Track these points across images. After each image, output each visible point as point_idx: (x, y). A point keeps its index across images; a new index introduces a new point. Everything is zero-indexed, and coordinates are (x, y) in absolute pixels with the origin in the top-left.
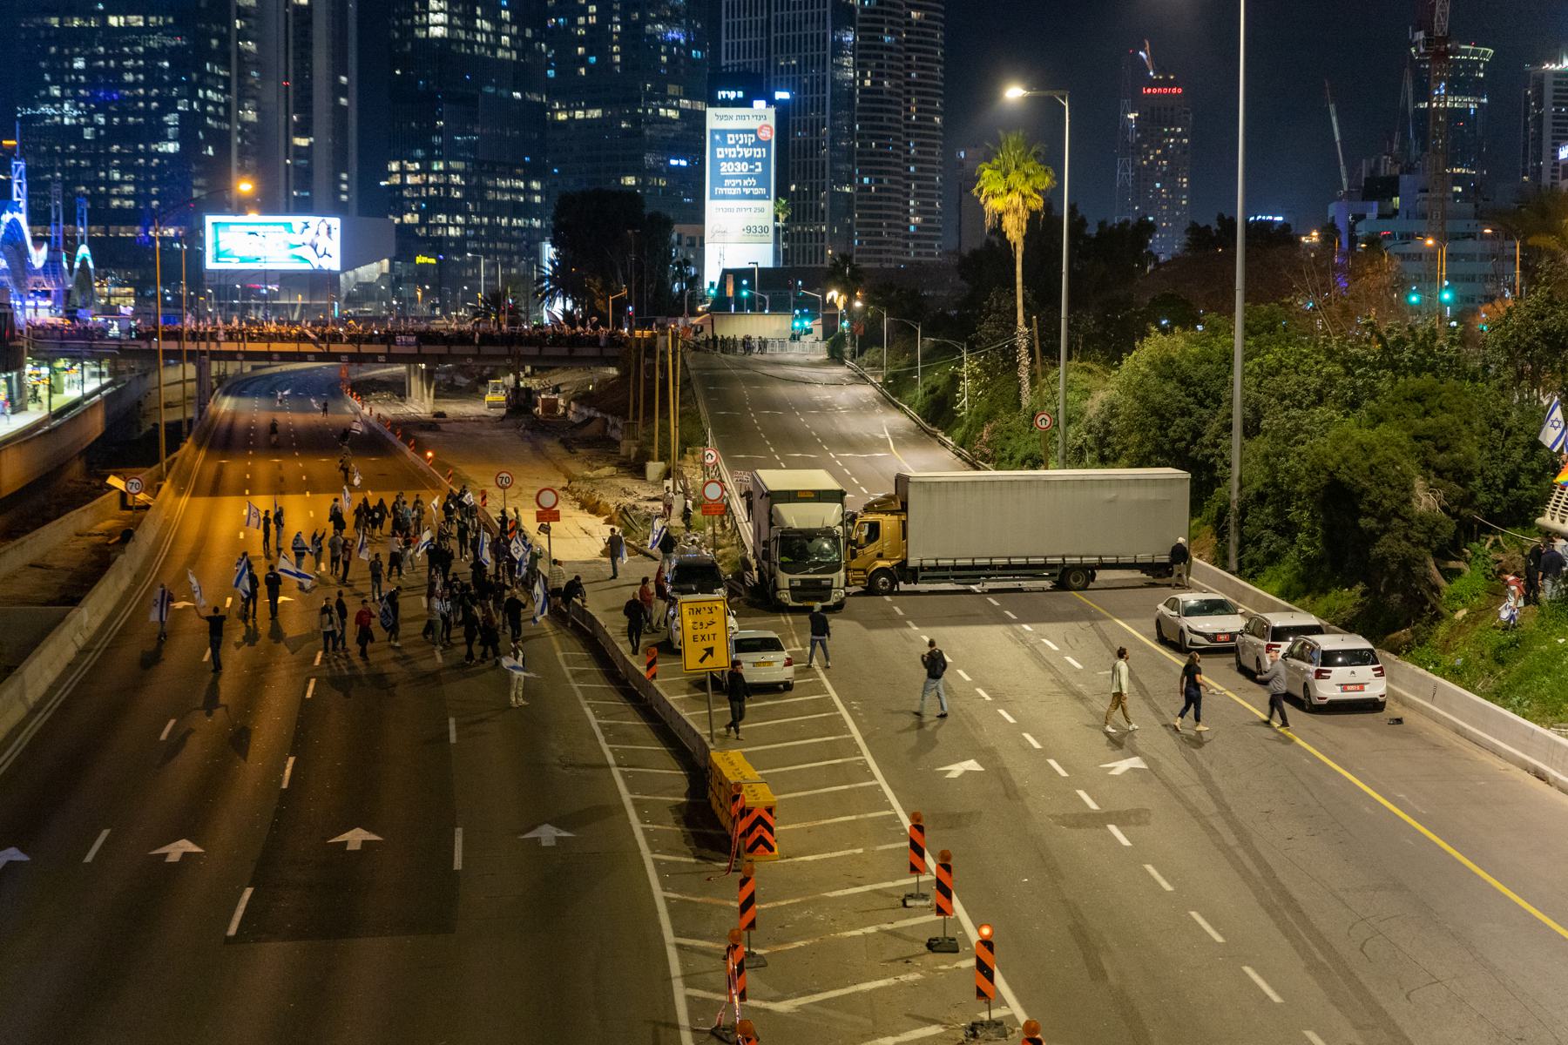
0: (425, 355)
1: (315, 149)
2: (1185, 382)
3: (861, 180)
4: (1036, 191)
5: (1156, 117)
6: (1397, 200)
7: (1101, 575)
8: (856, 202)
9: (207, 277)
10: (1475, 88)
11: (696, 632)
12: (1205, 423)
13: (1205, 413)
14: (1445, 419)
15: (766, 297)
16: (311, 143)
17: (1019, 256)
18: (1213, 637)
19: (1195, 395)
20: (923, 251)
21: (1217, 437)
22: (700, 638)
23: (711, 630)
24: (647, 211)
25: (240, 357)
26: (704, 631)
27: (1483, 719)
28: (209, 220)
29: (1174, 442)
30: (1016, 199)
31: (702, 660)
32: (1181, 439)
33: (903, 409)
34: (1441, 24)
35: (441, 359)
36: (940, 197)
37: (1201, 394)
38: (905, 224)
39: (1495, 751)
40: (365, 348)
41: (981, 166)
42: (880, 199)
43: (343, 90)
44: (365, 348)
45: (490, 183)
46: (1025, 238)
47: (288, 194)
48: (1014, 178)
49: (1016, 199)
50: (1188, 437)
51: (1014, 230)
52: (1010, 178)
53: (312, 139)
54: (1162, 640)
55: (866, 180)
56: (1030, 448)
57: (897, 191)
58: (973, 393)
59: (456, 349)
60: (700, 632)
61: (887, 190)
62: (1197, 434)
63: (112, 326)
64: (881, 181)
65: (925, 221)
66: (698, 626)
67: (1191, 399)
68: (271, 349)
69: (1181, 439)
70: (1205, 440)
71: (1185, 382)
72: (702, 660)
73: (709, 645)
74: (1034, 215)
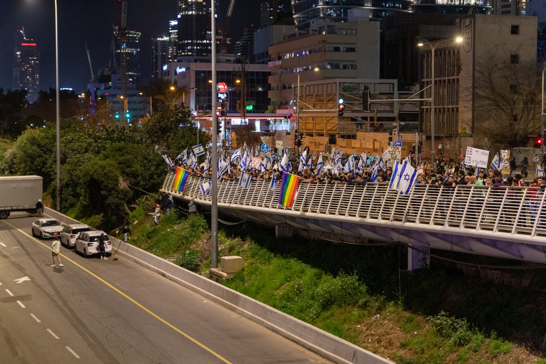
2: (39, 146)
5: (27, 53)
6: (110, 83)
7: (12, 214)
10: (134, 46)
12: (47, 160)
13: (47, 156)
14: (129, 157)
18: (52, 234)
19: (43, 150)
27: (144, 257)
29: (36, 166)
34: (124, 23)
39: (148, 268)
50: (41, 165)
54: (34, 235)
62: (45, 164)
69: (39, 165)
70: (47, 166)
71: (39, 146)
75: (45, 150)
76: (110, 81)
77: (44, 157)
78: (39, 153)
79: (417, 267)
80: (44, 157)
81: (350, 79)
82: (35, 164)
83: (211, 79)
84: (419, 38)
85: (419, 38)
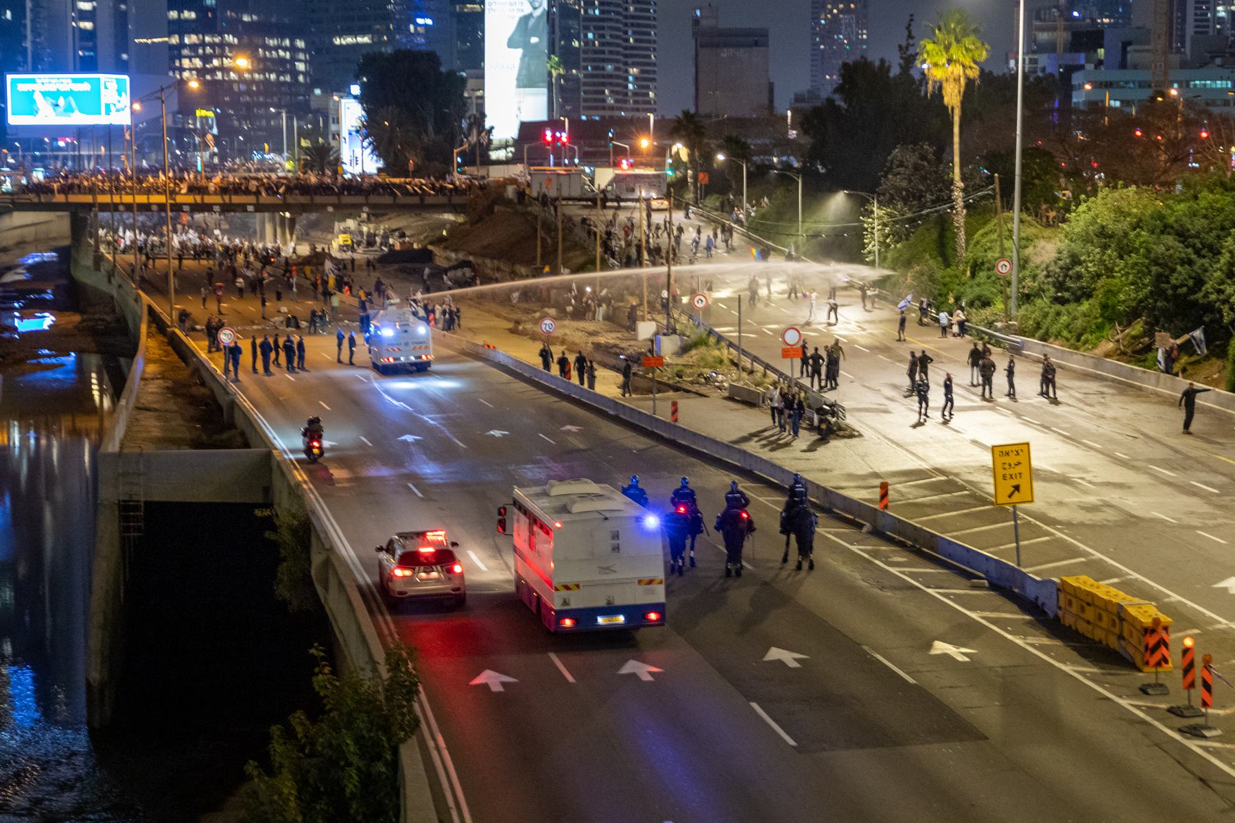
0: (290, 204)
1: (98, 12)
2: (1182, 235)
3: (586, 36)
4: (975, 62)
6: (1101, 52)
8: (582, 56)
9: (9, 131)
11: (1005, 472)
12: (1206, 270)
13: (1205, 261)
15: (576, 148)
16: (94, 8)
17: (957, 119)
19: (1193, 246)
20: (640, 99)
21: (1222, 283)
22: (1008, 477)
23: (1018, 469)
24: (443, 69)
25: (121, 208)
26: (1012, 471)
28: (10, 78)
29: (1175, 288)
30: (958, 70)
31: (1010, 496)
32: (1182, 286)
33: (779, 250)
35: (304, 208)
36: (655, 49)
37: (1199, 245)
38: (625, 75)
40: (236, 199)
41: (922, 43)
42: (603, 52)
44: (236, 199)
45: (260, 41)
46: (963, 103)
47: (75, 53)
48: (956, 52)
49: (958, 70)
50: (1191, 283)
51: (952, 97)
52: (952, 50)
53: (95, 3)
55: (590, 35)
56: (977, 290)
57: (618, 45)
58: (881, 239)
59: (319, 199)
60: (1008, 472)
61: (609, 44)
62: (1199, 282)
63: (5, 182)
64: (603, 36)
65: (642, 72)
66: (1007, 466)
67: (1190, 250)
68: (151, 201)
69: (1182, 286)
70: (1208, 286)
71: (1182, 235)
72: (1010, 496)
73: (1015, 482)
74: (970, 82)
75: (1199, 245)
76: (1101, 46)
77: (1198, 264)
78: (1183, 255)
79: (131, 449)
80: (1198, 264)
81: (364, 629)
82: (1173, 281)
83: (632, 166)
84: (63, 436)
85: (63, 436)
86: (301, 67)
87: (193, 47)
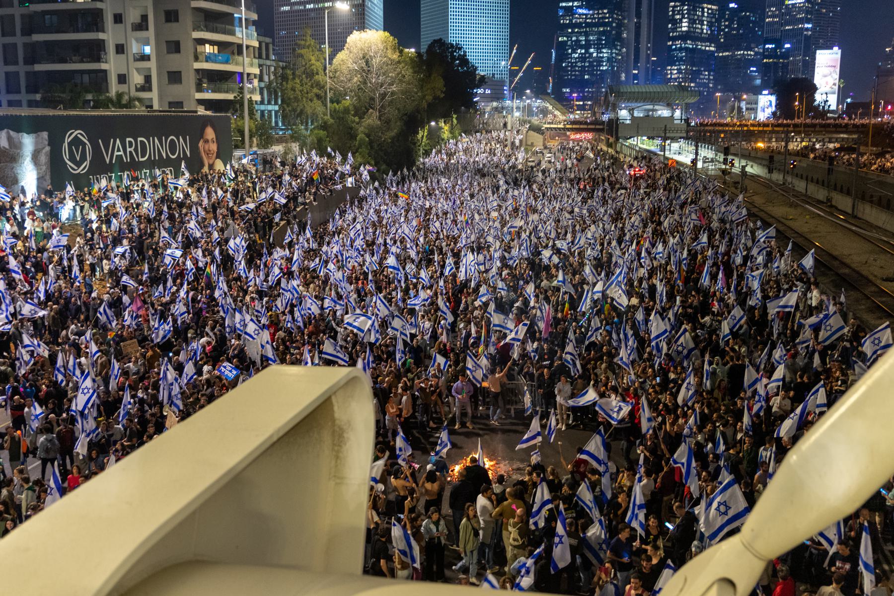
43: (648, 49)
86: (711, 85)
87: (675, 79)
